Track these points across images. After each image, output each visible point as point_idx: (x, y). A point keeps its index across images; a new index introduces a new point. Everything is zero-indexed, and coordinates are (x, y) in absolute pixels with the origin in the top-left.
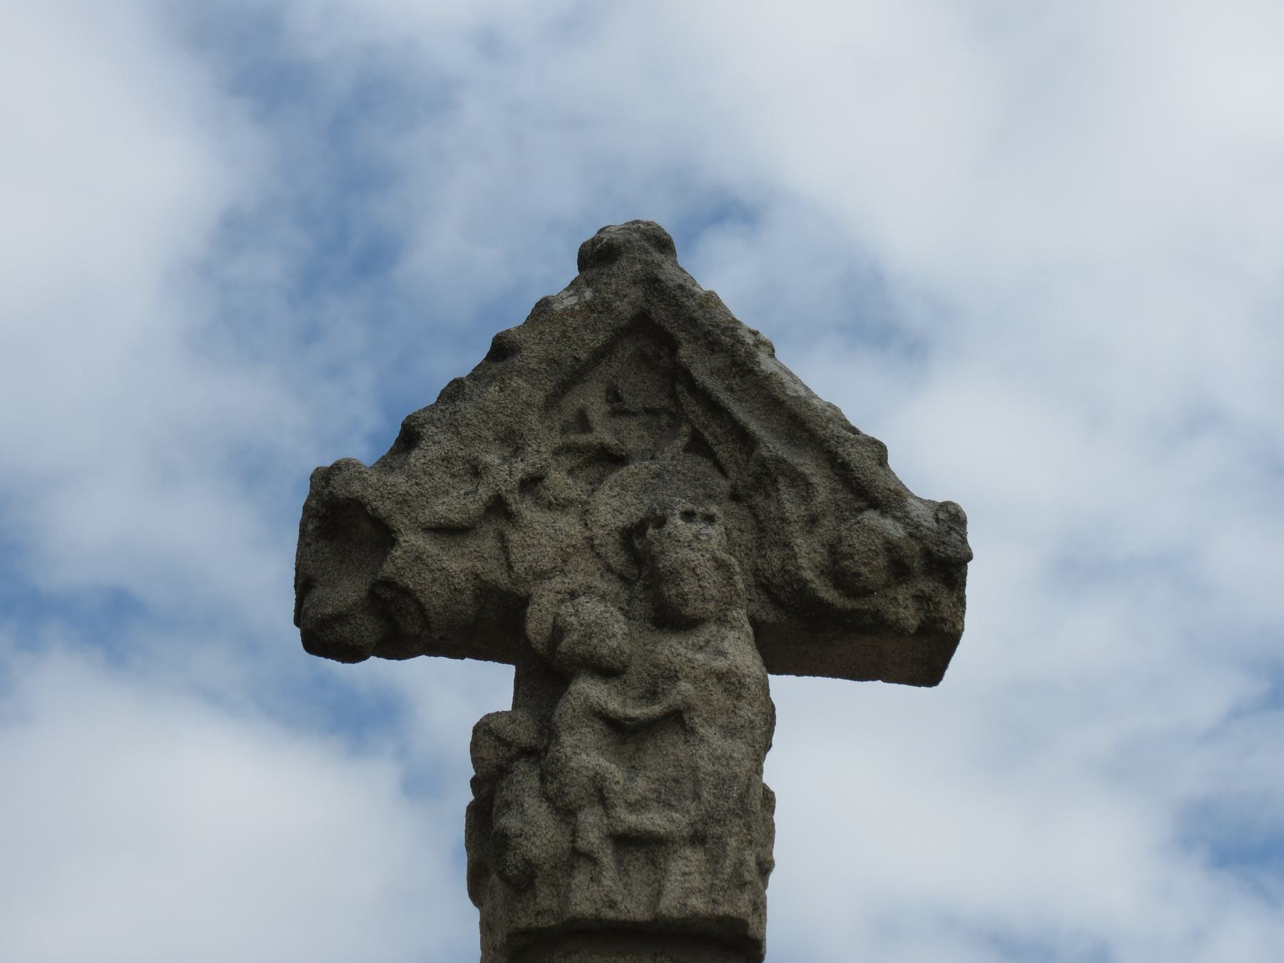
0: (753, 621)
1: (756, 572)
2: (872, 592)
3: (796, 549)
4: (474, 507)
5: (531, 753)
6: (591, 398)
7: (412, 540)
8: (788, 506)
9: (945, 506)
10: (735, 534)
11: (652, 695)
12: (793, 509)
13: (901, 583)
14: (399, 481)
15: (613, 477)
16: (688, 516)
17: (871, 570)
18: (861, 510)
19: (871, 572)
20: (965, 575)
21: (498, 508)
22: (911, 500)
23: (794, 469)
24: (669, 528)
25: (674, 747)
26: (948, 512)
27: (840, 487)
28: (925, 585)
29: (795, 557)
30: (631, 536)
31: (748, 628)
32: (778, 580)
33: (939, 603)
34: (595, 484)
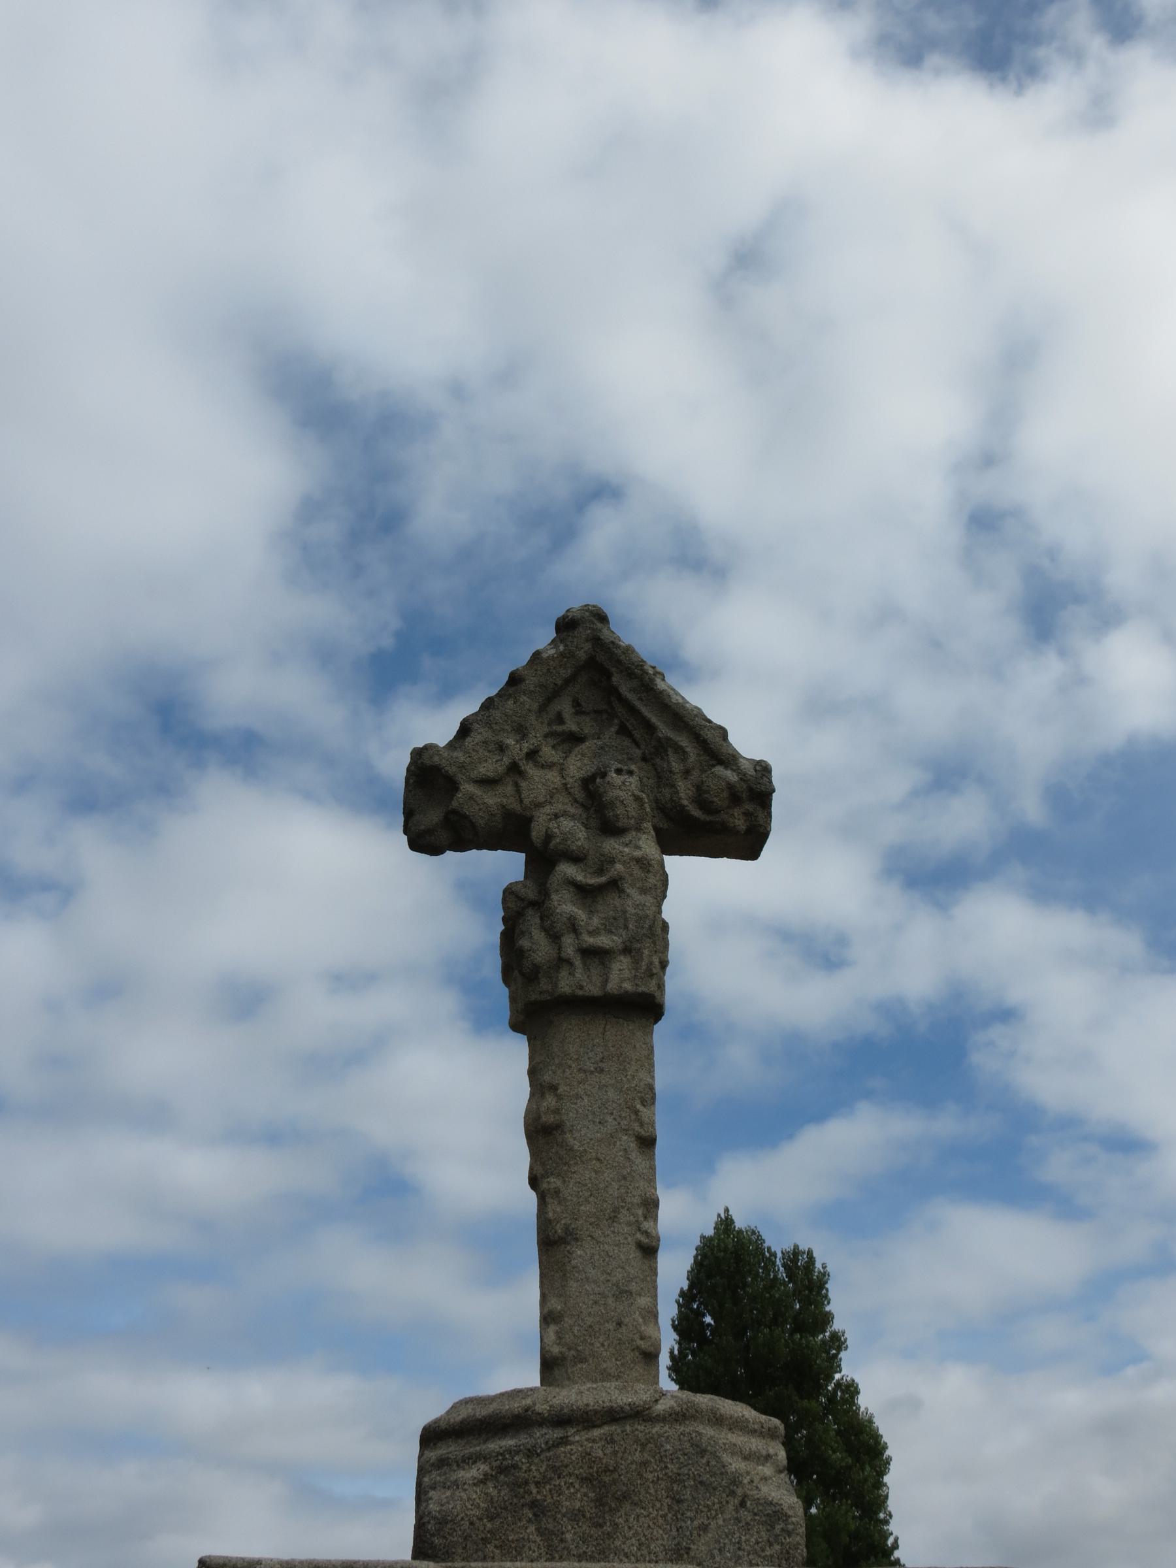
0: (655, 828)
1: (657, 801)
4: (501, 768)
5: (536, 905)
7: (467, 788)
9: (759, 762)
10: (645, 780)
11: (600, 871)
12: (676, 766)
14: (459, 755)
15: (577, 749)
16: (619, 771)
17: (720, 799)
18: (714, 766)
21: (514, 769)
24: (608, 779)
25: (613, 900)
28: (749, 807)
29: (677, 792)
30: (587, 782)
31: (653, 833)
34: (567, 754)
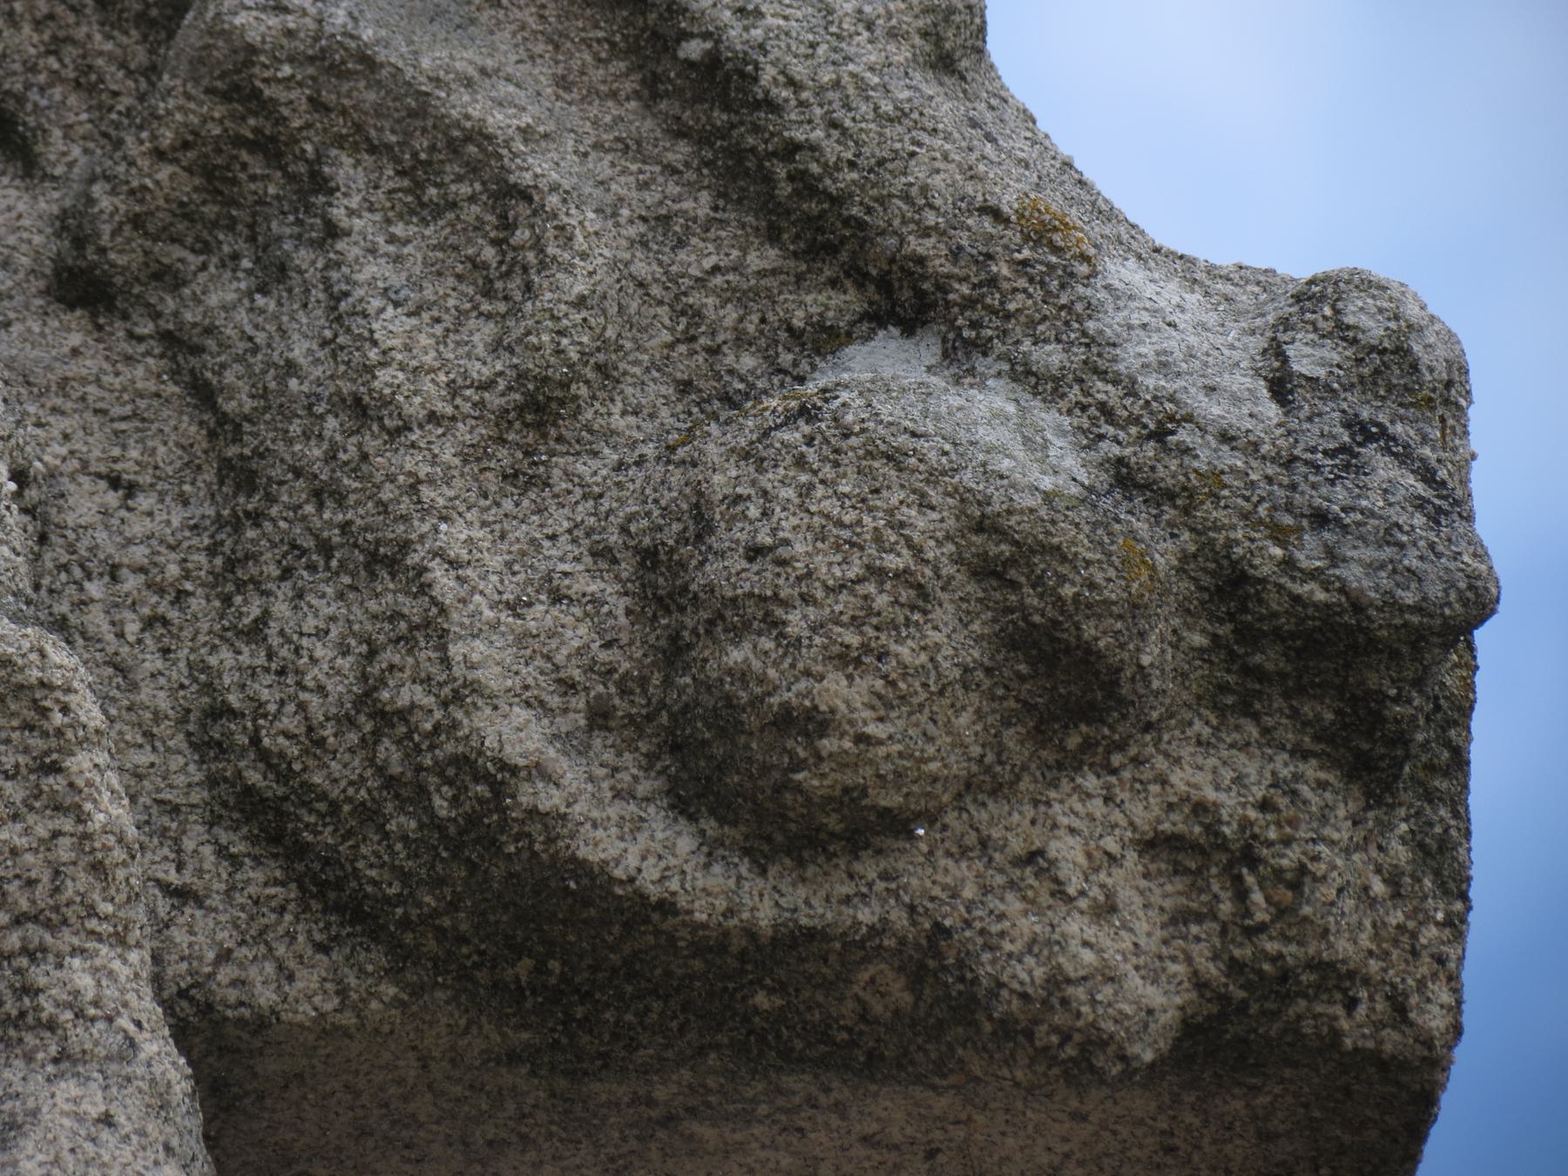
0: (196, 1021)
1: (211, 725)
2: (898, 825)
3: (443, 581)
8: (391, 326)
9: (1319, 300)
10: (85, 504)
12: (413, 329)
13: (1070, 764)
17: (888, 693)
18: (825, 340)
19: (883, 704)
20: (1464, 708)
22: (1122, 272)
23: (418, 108)
26: (1343, 332)
27: (701, 205)
28: (1216, 774)
29: (432, 629)
31: (161, 1056)
32: (339, 772)
33: (1299, 879)
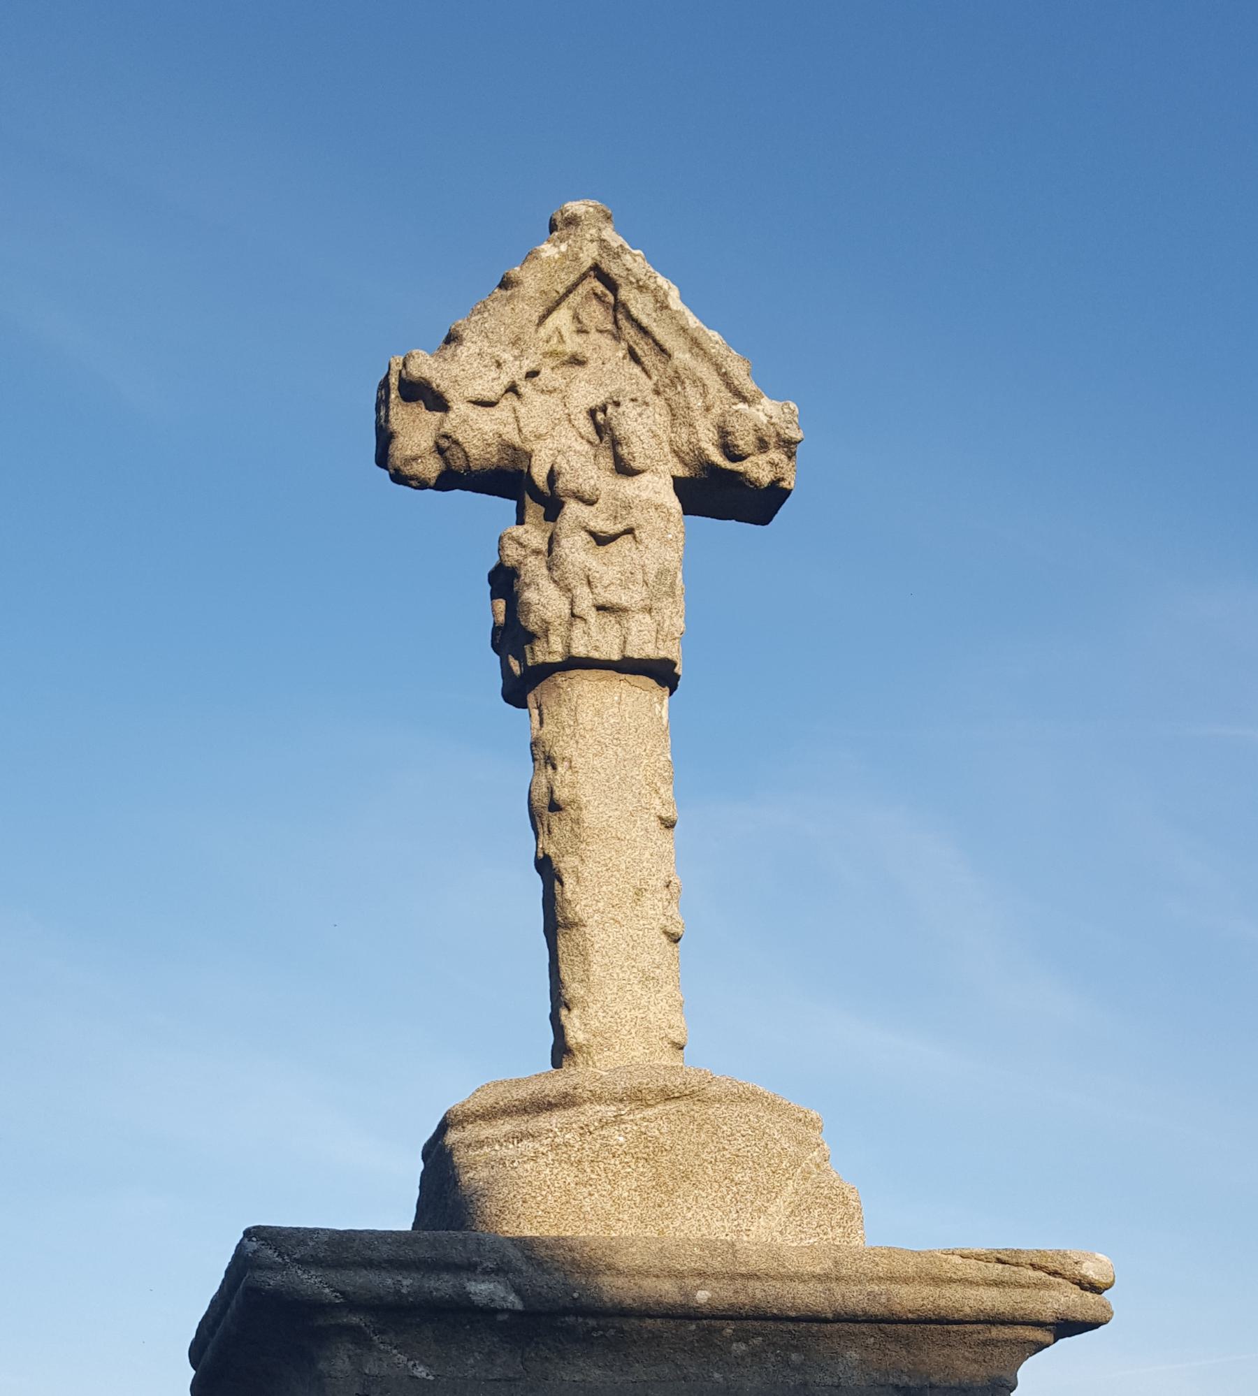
4: (499, 389)
6: (562, 318)
7: (460, 408)
17: (745, 442)
21: (513, 389)
32: (685, 448)
